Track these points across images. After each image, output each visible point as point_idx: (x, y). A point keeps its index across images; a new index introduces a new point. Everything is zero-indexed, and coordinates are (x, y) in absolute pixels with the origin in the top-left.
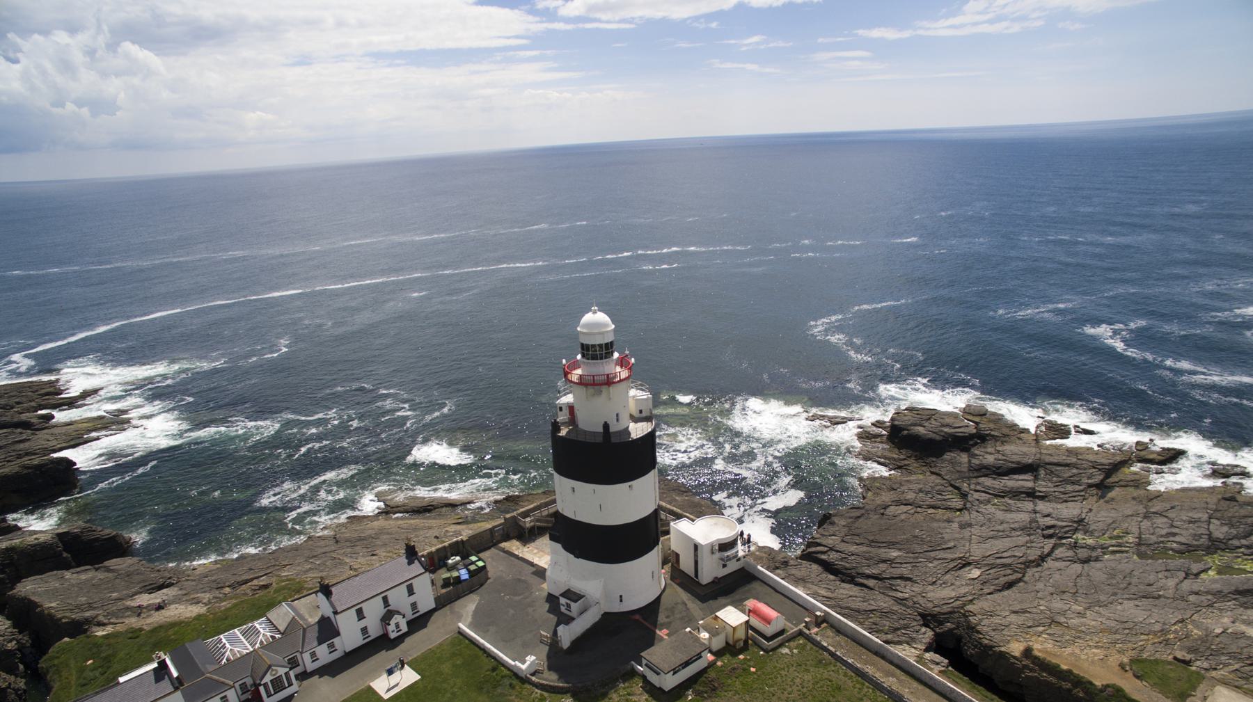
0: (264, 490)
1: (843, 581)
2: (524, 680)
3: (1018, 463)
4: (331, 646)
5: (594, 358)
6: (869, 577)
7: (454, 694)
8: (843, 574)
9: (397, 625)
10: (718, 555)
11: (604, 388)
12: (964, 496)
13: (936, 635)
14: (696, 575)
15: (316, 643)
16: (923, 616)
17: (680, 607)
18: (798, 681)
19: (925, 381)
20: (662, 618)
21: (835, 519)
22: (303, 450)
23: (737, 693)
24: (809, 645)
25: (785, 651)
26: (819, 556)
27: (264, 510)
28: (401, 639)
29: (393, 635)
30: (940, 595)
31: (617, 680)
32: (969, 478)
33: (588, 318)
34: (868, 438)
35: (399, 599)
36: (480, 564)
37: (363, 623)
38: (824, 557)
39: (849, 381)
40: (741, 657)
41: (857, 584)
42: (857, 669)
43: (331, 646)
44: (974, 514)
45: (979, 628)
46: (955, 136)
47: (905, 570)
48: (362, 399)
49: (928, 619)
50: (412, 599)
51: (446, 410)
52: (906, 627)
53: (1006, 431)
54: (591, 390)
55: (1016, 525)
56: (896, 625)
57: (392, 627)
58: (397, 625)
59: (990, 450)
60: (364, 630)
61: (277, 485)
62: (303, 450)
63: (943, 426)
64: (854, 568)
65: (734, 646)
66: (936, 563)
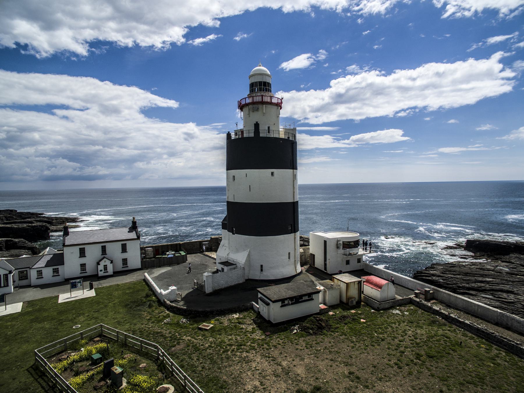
2: (161, 303)
4: (56, 271)
9: (105, 267)
10: (341, 251)
11: (260, 106)
14: (325, 269)
23: (343, 334)
24: (420, 311)
29: (101, 274)
35: (114, 251)
37: (83, 261)
40: (353, 311)
42: (478, 330)
43: (56, 271)
46: (496, 96)
50: (125, 256)
57: (101, 267)
58: (105, 267)
60: (83, 266)
65: (347, 304)
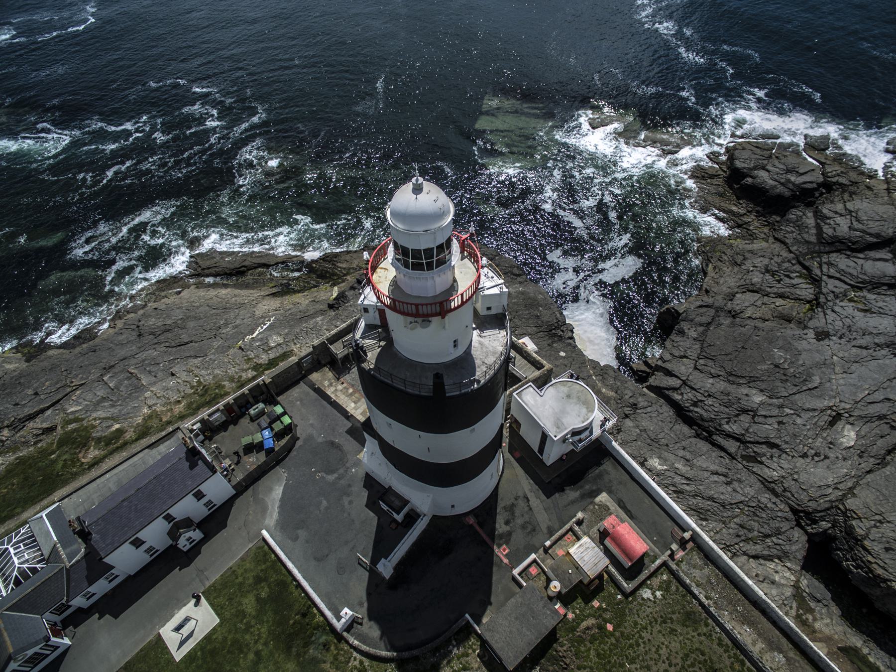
0: (74, 235)
1: (698, 436)
3: (877, 235)
5: (417, 267)
6: (729, 436)
7: (258, 653)
8: (699, 426)
11: (436, 320)
12: (816, 282)
13: (811, 538)
14: (541, 450)
15: (86, 584)
16: (794, 511)
17: (521, 503)
18: (663, 651)
19: (761, 94)
20: (501, 527)
21: (684, 325)
22: (110, 174)
25: (647, 594)
26: (670, 393)
27: (76, 265)
28: (196, 549)
30: (817, 478)
31: (448, 642)
32: (820, 254)
33: (404, 198)
34: (703, 178)
36: (287, 420)
38: (677, 397)
39: (683, 89)
41: (714, 444)
44: (831, 316)
45: (867, 543)
47: (768, 429)
48: (168, 104)
49: (801, 516)
51: (255, 119)
52: (778, 533)
53: (853, 176)
54: (410, 319)
55: (880, 340)
56: (766, 530)
59: (839, 207)
61: (89, 228)
62: (110, 174)
63: (788, 171)
64: (712, 420)
66: (806, 416)
